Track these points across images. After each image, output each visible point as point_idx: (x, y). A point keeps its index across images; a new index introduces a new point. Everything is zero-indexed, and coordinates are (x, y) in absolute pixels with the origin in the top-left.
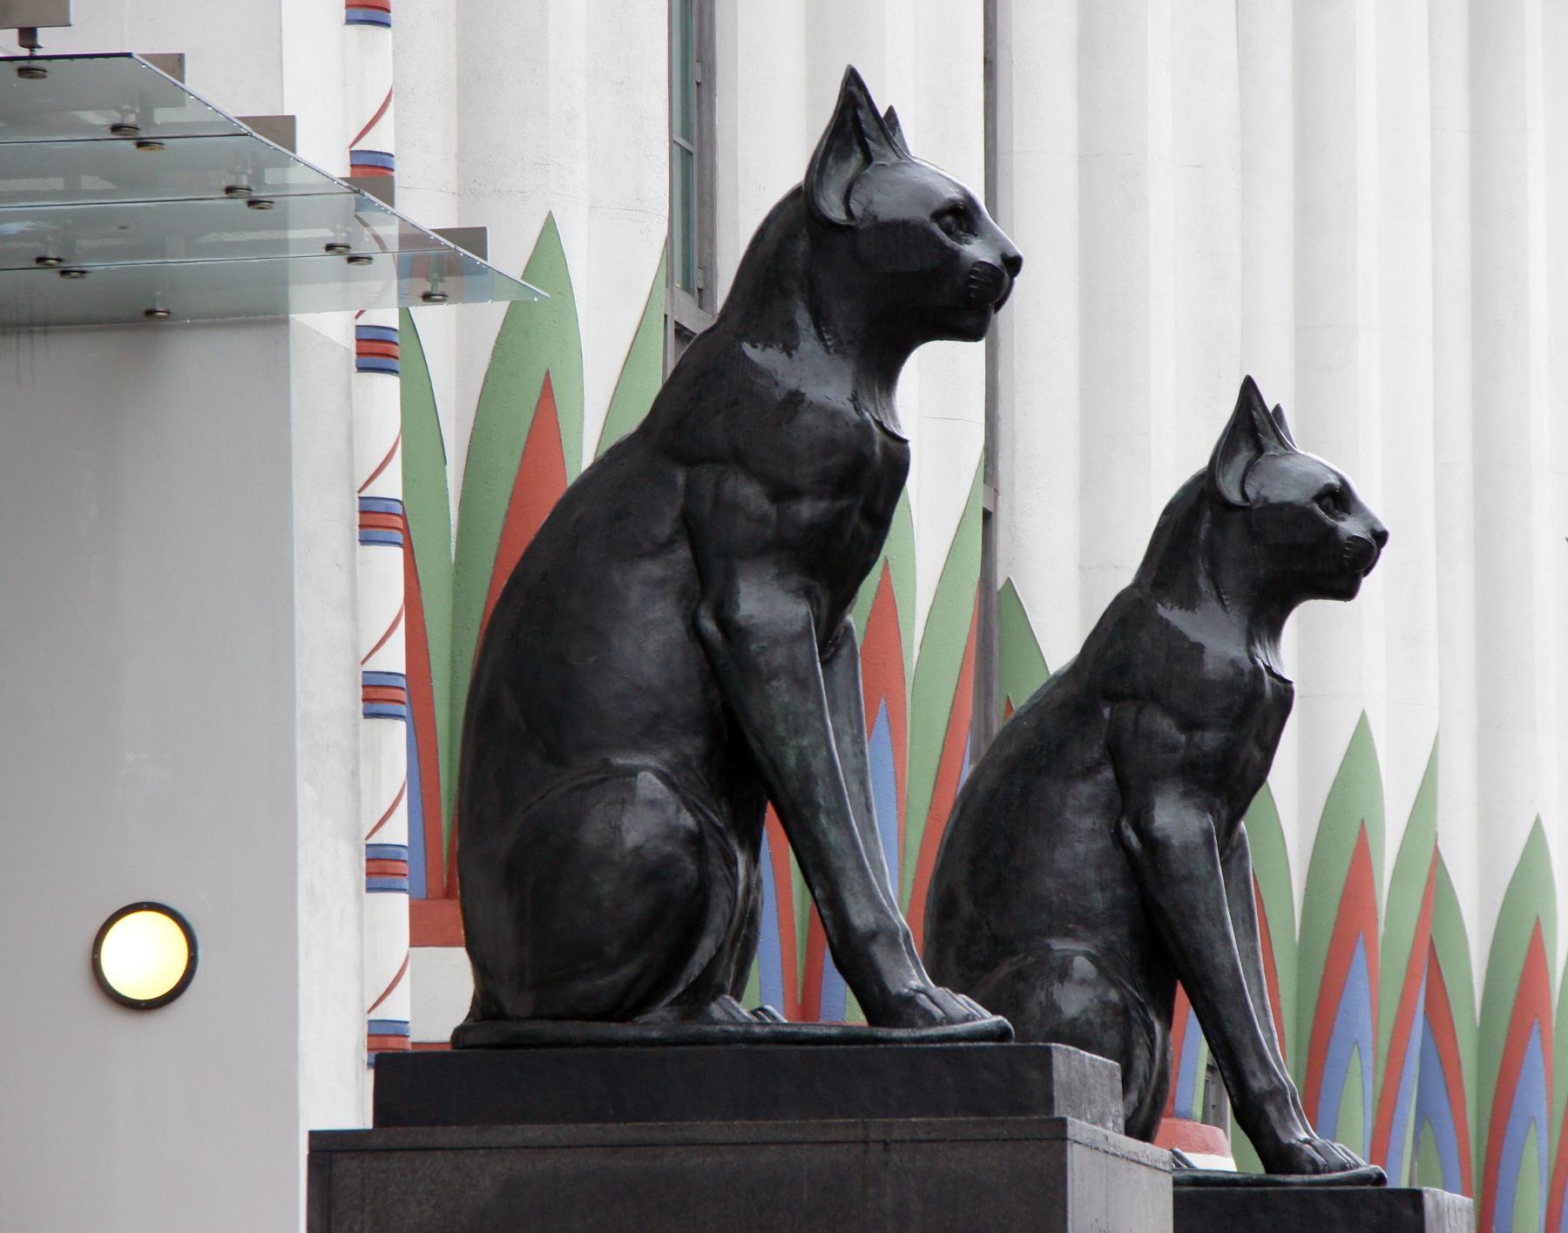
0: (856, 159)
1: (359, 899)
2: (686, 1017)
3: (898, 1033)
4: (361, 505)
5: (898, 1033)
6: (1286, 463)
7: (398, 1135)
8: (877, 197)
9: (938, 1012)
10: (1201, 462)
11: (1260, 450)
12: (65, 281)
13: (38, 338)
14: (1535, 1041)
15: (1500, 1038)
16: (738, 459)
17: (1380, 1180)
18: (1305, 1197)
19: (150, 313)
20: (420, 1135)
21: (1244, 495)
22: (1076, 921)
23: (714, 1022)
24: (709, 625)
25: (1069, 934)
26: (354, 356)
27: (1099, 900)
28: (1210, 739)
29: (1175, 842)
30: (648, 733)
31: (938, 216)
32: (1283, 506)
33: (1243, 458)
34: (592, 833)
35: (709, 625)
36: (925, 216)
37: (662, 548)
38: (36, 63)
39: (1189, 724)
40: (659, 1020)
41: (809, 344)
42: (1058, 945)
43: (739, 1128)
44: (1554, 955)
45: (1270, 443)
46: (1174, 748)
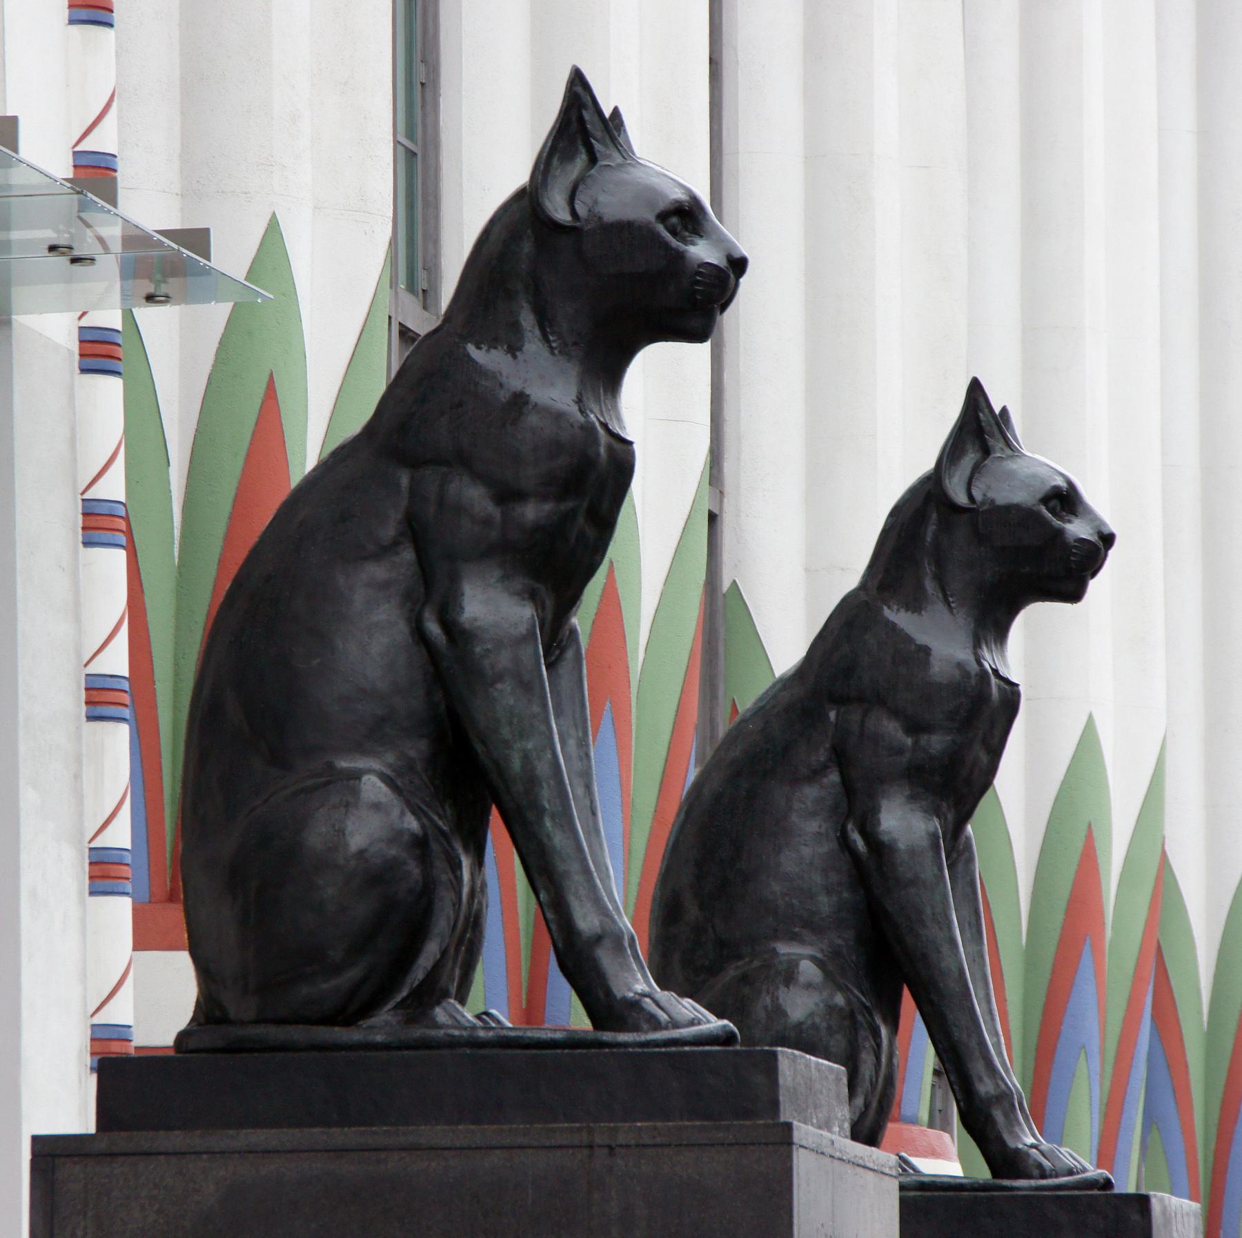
0: (581, 159)
2: (410, 1021)
3: (623, 1037)
5: (623, 1037)
6: (1012, 465)
7: (122, 1140)
8: (602, 198)
9: (663, 1016)
10: (927, 464)
11: (986, 451)
17: (1108, 1184)
21: (971, 497)
23: (440, 1027)
24: (433, 628)
25: (794, 938)
26: (77, 357)
27: (824, 904)
29: (902, 846)
33: (969, 459)
34: (316, 836)
35: (433, 628)
36: (650, 216)
39: (915, 727)
41: (533, 345)
42: (784, 949)
45: (997, 445)
46: (900, 751)
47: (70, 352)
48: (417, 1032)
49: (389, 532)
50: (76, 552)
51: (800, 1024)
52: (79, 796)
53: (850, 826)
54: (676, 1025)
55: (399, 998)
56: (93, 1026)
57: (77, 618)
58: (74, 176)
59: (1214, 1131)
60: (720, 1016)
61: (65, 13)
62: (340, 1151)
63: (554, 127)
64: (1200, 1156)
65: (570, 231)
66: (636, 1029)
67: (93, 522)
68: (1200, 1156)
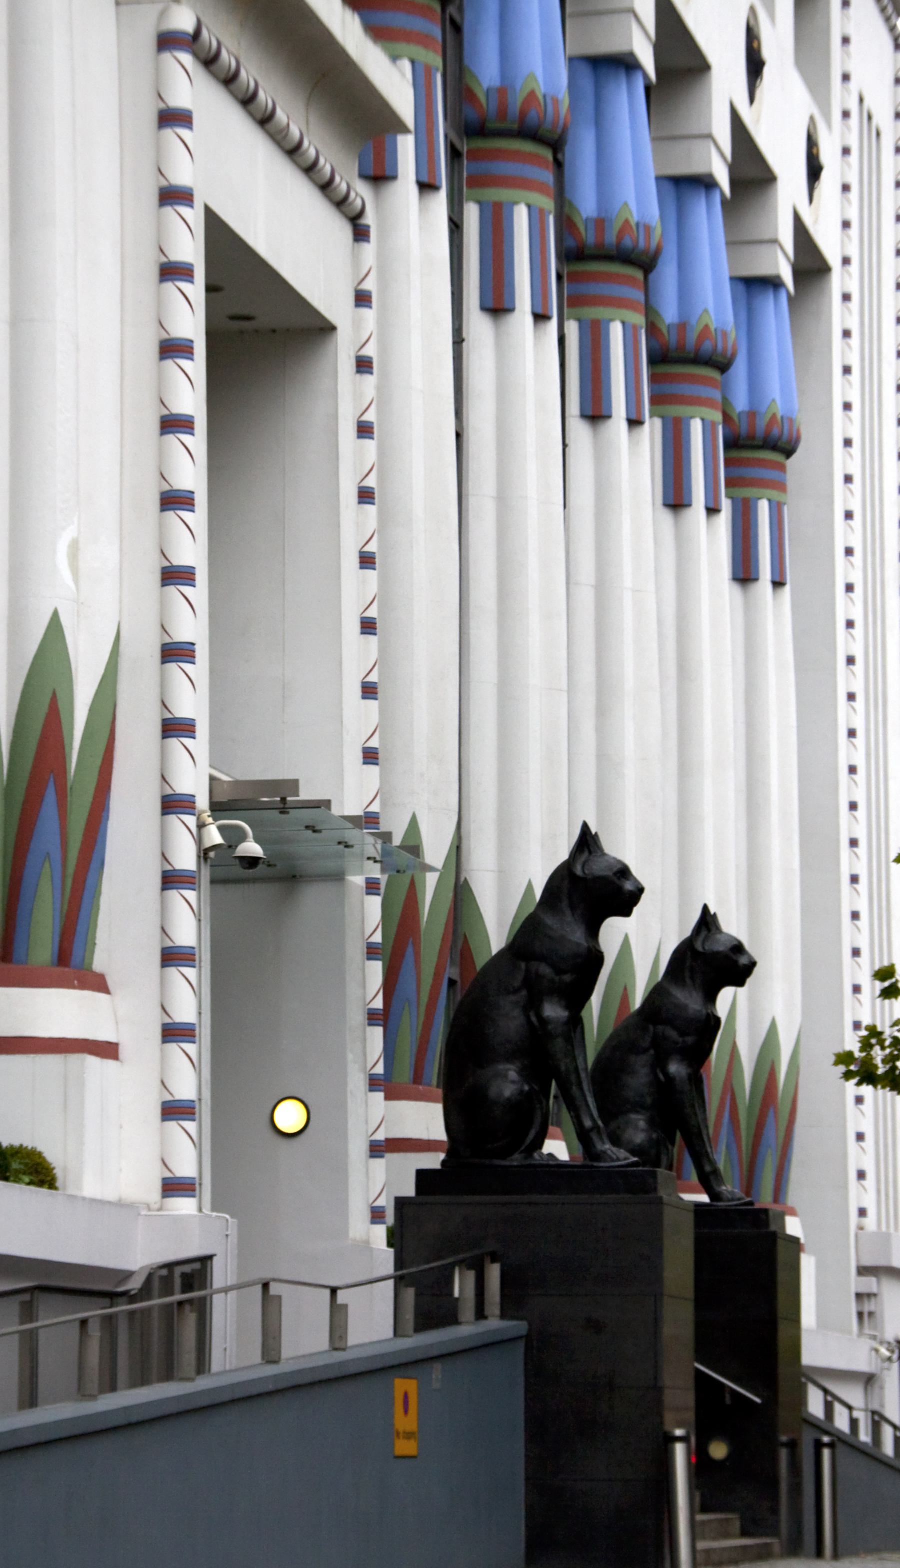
0: (586, 854)
1: (366, 1095)
2: (526, 1158)
3: (602, 1165)
4: (367, 945)
5: (602, 1165)
6: (719, 936)
7: (422, 1199)
8: (594, 867)
9: (615, 1157)
10: (688, 933)
11: (709, 930)
12: (269, 868)
13: (251, 886)
14: (771, 1114)
15: (757, 1112)
16: (543, 959)
17: (751, 1204)
18: (726, 1212)
19: (294, 877)
20: (431, 1199)
21: (704, 948)
22: (638, 1107)
23: (537, 1160)
24: (534, 1019)
25: (637, 1113)
26: (365, 889)
27: (649, 1100)
28: (690, 1040)
29: (678, 1079)
30: (510, 1058)
31: (615, 874)
32: (718, 953)
33: (704, 933)
34: (493, 1092)
35: (534, 1019)
36: (610, 874)
37: (516, 991)
38: (285, 810)
39: (683, 1034)
40: (516, 1160)
41: (569, 917)
42: (633, 1116)
43: (545, 1198)
44: (780, 1072)
45: (714, 929)
46: (677, 1043)
47: (363, 887)
48: (528, 1162)
49: (517, 984)
50: (364, 961)
51: (640, 1145)
52: (365, 1055)
53: (658, 1071)
54: (618, 1160)
55: (523, 1148)
56: (371, 1141)
57: (364, 987)
58: (425, 874)
59: (750, 1147)
60: (634, 1156)
61: (362, 760)
62: (504, 1205)
63: (577, 841)
64: (744, 1156)
65: (583, 880)
66: (605, 1161)
67: (371, 951)
68: (744, 1156)
